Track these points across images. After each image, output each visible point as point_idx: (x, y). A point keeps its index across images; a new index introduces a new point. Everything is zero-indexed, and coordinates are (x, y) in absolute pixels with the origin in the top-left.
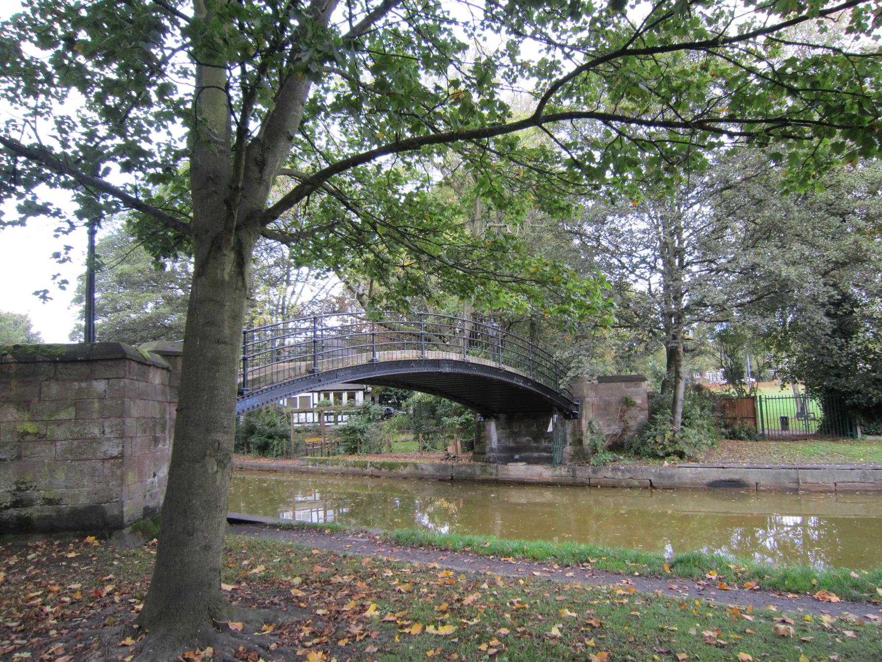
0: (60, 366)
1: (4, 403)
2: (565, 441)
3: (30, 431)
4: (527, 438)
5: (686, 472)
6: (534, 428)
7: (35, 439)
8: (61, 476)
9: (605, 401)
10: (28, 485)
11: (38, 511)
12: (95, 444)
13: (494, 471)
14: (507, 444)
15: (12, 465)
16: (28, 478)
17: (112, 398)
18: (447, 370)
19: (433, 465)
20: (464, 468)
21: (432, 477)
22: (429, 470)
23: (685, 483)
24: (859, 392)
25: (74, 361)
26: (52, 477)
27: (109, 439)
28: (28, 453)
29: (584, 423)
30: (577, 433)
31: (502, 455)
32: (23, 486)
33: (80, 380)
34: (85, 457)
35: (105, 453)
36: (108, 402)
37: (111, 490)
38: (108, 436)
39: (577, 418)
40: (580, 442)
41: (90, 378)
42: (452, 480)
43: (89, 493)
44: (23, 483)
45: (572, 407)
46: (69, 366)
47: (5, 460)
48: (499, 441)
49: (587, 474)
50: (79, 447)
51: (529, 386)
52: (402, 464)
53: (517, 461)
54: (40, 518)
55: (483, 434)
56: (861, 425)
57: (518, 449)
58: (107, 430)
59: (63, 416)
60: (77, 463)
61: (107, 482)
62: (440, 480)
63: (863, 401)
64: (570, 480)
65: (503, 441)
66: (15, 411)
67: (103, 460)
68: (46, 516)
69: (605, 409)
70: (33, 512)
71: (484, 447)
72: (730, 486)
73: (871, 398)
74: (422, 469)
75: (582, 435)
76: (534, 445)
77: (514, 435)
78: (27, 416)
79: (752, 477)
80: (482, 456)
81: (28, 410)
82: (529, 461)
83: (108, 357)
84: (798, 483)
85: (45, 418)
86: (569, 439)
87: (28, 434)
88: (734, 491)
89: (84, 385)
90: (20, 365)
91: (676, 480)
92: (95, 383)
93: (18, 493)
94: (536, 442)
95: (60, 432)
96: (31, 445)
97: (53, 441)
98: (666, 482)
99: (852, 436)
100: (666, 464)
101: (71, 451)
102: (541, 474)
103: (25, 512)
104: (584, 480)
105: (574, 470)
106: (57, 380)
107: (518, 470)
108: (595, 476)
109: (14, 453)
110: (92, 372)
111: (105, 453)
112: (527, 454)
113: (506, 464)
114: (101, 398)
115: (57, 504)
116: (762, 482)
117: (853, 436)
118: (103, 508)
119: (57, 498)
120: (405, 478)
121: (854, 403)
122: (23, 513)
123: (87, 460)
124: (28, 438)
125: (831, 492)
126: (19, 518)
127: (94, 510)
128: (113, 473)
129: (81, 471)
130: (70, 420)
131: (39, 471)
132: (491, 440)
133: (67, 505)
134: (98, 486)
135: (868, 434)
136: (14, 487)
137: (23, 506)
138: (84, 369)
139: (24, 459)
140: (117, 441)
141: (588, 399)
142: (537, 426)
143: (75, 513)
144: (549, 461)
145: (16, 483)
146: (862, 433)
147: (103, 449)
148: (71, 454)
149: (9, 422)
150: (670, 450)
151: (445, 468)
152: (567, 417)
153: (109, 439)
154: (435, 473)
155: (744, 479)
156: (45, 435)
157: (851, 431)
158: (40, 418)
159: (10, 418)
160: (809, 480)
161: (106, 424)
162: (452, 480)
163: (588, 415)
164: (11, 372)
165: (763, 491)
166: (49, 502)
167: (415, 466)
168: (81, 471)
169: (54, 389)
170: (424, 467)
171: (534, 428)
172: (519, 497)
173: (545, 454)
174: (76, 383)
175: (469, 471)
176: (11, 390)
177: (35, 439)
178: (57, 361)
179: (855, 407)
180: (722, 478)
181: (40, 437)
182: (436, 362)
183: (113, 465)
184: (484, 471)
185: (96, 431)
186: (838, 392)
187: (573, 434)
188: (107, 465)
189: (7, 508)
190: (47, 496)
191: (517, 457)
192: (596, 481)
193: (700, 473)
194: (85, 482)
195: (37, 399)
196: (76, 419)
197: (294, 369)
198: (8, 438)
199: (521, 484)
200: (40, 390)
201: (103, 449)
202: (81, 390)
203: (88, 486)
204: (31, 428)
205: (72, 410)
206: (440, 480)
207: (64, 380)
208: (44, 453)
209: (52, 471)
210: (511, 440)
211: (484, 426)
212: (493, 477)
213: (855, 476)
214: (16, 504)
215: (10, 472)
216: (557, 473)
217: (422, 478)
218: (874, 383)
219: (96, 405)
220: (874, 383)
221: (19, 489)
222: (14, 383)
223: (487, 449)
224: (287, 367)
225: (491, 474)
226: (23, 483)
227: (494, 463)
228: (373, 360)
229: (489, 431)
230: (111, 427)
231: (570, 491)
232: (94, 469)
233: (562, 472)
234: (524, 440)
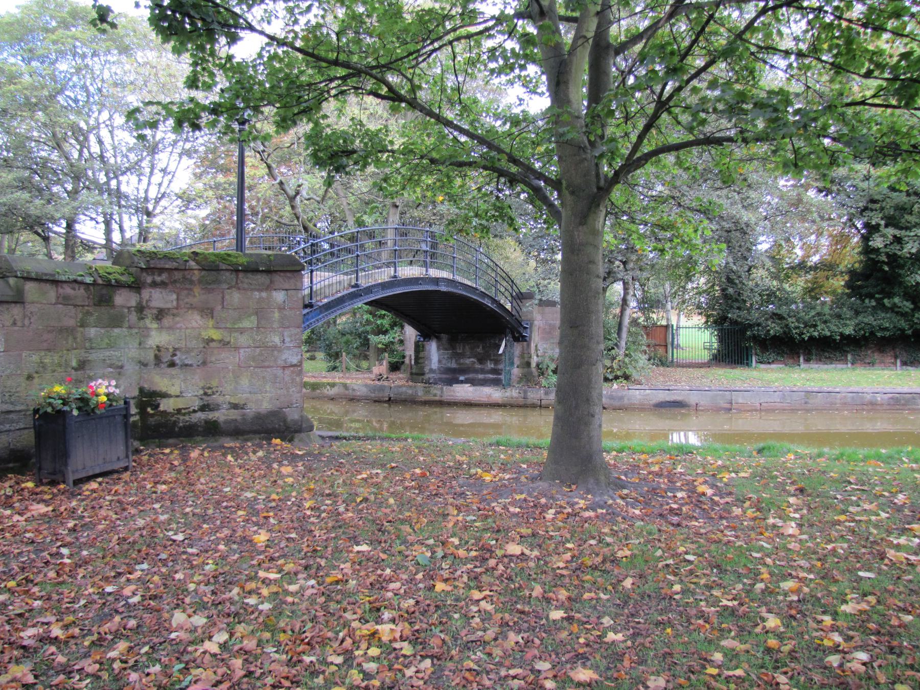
0: (241, 275)
1: (189, 309)
2: (512, 364)
3: (215, 337)
5: (636, 394)
6: (480, 350)
7: (219, 346)
8: (245, 382)
9: (550, 325)
10: (214, 390)
12: (276, 352)
13: (439, 393)
14: (449, 365)
15: (198, 371)
16: (214, 383)
18: (443, 288)
19: (366, 385)
20: (404, 389)
23: (634, 404)
24: (759, 325)
25: (256, 271)
26: (237, 383)
28: (213, 359)
29: (533, 345)
30: (526, 355)
31: (444, 376)
32: (209, 392)
33: (260, 290)
34: (266, 364)
35: (285, 361)
36: (287, 313)
38: (287, 345)
39: (526, 341)
40: (528, 364)
41: (269, 288)
42: (389, 401)
43: (271, 399)
44: (210, 388)
45: (521, 330)
46: (250, 275)
47: (191, 365)
48: (440, 361)
49: (538, 396)
50: (261, 354)
51: (493, 307)
52: (328, 384)
53: (462, 382)
54: (226, 422)
55: (421, 355)
56: (756, 354)
57: (463, 371)
58: (287, 339)
59: (246, 324)
60: (259, 370)
61: (288, 389)
62: (375, 401)
63: (762, 334)
64: (521, 401)
65: (444, 361)
66: (198, 317)
67: (284, 368)
68: (233, 420)
69: (550, 333)
70: (220, 416)
71: (423, 368)
72: (670, 407)
73: (769, 331)
74: (354, 390)
76: (478, 366)
77: (456, 356)
78: (211, 323)
79: (693, 398)
80: (421, 377)
81: (212, 318)
82: (473, 382)
83: (289, 268)
84: (731, 403)
85: (228, 325)
86: (517, 361)
87: (213, 340)
88: (676, 410)
89: (264, 294)
90: (203, 273)
91: (626, 401)
92: (275, 294)
93: (205, 398)
95: (243, 340)
96: (216, 351)
97: (237, 348)
98: (617, 403)
99: (747, 364)
100: (615, 386)
101: (254, 359)
102: (490, 396)
103: (211, 416)
105: (525, 392)
106: (239, 289)
107: (464, 391)
108: (547, 397)
110: (271, 282)
112: (471, 376)
113: (451, 385)
114: (281, 309)
115: (242, 408)
116: (702, 403)
117: (748, 365)
118: (284, 413)
119: (242, 402)
120: (332, 399)
121: (754, 335)
124: (212, 345)
125: (756, 410)
127: (276, 414)
128: (293, 380)
129: (264, 378)
130: (252, 328)
131: (224, 377)
132: (431, 360)
133: (252, 410)
134: (279, 392)
135: (761, 363)
136: (201, 392)
137: (210, 410)
138: (262, 279)
140: (296, 350)
141: (536, 323)
142: (483, 348)
143: (259, 417)
144: (496, 383)
145: (203, 388)
146: (757, 362)
148: (254, 361)
149: (193, 328)
150: (619, 373)
151: (382, 388)
152: (516, 339)
153: (289, 348)
154: (369, 394)
155: (687, 400)
156: (229, 343)
157: (747, 359)
158: (223, 326)
159: (194, 324)
160: (740, 401)
161: (286, 334)
162: (389, 401)
165: (702, 411)
166: (235, 406)
167: (345, 386)
168: (264, 378)
169: (235, 297)
170: (356, 388)
171: (480, 350)
172: (464, 417)
173: (491, 376)
174: (257, 293)
175: (410, 392)
176: (195, 296)
177: (219, 346)
178: (239, 271)
179: (755, 338)
180: (668, 399)
181: (225, 344)
182: (436, 281)
183: (293, 372)
184: (427, 392)
185: (277, 340)
186: (741, 323)
187: (522, 356)
188: (287, 372)
189: (194, 411)
190: (233, 401)
191: (462, 378)
193: (648, 395)
194: (268, 388)
195: (220, 307)
196: (258, 328)
198: (193, 344)
199: (468, 405)
200: (223, 298)
202: (260, 300)
203: (270, 392)
204: (215, 335)
205: (254, 318)
206: (375, 401)
207: (244, 289)
208: (229, 359)
209: (237, 377)
210: (454, 361)
211: (423, 347)
212: (437, 398)
213: (776, 398)
214: (203, 408)
215: (197, 377)
217: (352, 399)
218: (771, 317)
219: (277, 315)
220: (771, 317)
221: (205, 394)
222: (197, 290)
223: (426, 370)
224: (334, 281)
225: (435, 395)
226: (210, 388)
227: (435, 384)
228: (395, 277)
229: (429, 351)
230: (291, 336)
231: (521, 412)
232: (276, 377)
233: (513, 393)
234: (468, 361)
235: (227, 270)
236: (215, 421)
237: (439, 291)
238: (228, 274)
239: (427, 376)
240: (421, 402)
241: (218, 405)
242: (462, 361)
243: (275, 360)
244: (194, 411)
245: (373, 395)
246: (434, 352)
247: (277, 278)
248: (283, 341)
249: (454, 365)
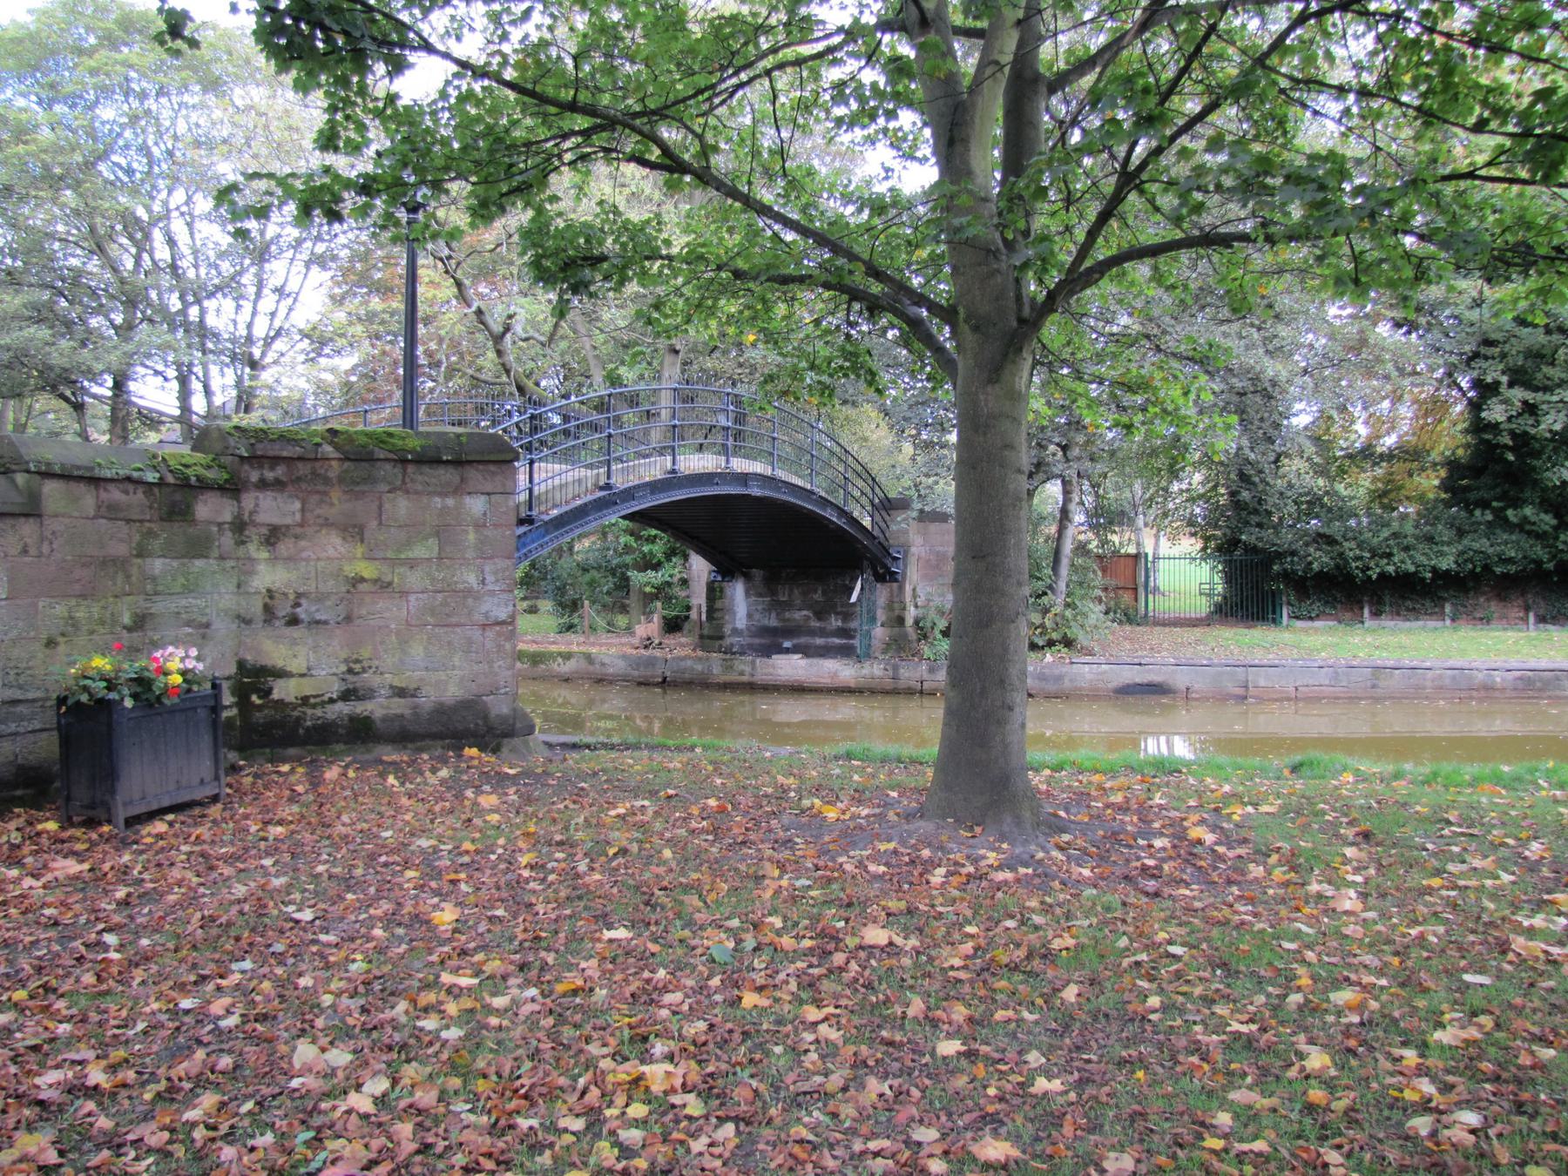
0: (411, 469)
1: (322, 526)
2: (873, 619)
3: (366, 575)
4: (805, 612)
6: (818, 596)
8: (417, 651)
10: (366, 664)
11: (382, 707)
12: (470, 601)
13: (748, 669)
14: (766, 622)
16: (365, 653)
17: (495, 526)
18: (756, 491)
19: (624, 657)
20: (689, 663)
21: (625, 679)
22: (617, 666)
23: (1080, 689)
24: (1293, 553)
25: (437, 462)
27: (492, 593)
28: (364, 612)
29: (908, 588)
31: (757, 641)
32: (357, 667)
33: (443, 495)
34: (454, 620)
35: (486, 615)
37: (496, 674)
38: (490, 587)
39: (896, 581)
40: (901, 621)
41: (459, 490)
43: (462, 679)
44: (357, 661)
45: (888, 562)
46: (426, 469)
47: (326, 623)
48: (749, 616)
49: (918, 675)
50: (445, 604)
51: (841, 522)
52: (560, 654)
53: (788, 651)
54: (385, 719)
55: (718, 604)
56: (1289, 603)
57: (789, 632)
58: (490, 578)
59: (419, 552)
60: (442, 630)
61: (491, 663)
62: (640, 684)
63: (1299, 569)
64: (888, 684)
65: (757, 616)
68: (397, 716)
69: (937, 567)
70: (375, 708)
71: (721, 627)
73: (1310, 563)
74: (603, 664)
75: (904, 609)
76: (815, 624)
77: (778, 606)
78: (360, 550)
79: (1181, 679)
80: (717, 643)
81: (362, 541)
82: (807, 651)
83: (487, 458)
84: (1246, 687)
85: (390, 554)
86: (881, 616)
87: (363, 580)
88: (1153, 699)
89: (450, 502)
90: (347, 464)
91: (1067, 684)
92: (468, 500)
93: (350, 677)
94: (820, 619)
95: (414, 579)
96: (368, 599)
97: (404, 594)
98: (1051, 687)
99: (1274, 621)
100: (1049, 658)
102: (835, 674)
103: (360, 708)
104: (913, 684)
105: (896, 668)
106: (407, 492)
107: (790, 667)
109: (342, 610)
111: (486, 615)
112: (803, 640)
113: (769, 656)
114: (479, 526)
115: (413, 696)
117: (1275, 622)
118: (485, 703)
120: (567, 680)
121: (1285, 570)
122: (358, 710)
123: (457, 625)
124: (363, 587)
125: (1289, 699)
126: (353, 719)
127: (470, 705)
129: (449, 643)
130: (428, 560)
131: (382, 643)
132: (734, 614)
133: (429, 698)
134: (476, 667)
135: (1297, 618)
136: (343, 668)
137: (359, 699)
138: (447, 475)
139: (358, 622)
140: (505, 596)
141: (913, 549)
142: (824, 593)
143: (441, 710)
144: (846, 652)
145: (346, 661)
146: (1290, 617)
147: (484, 608)
148: (433, 615)
150: (1055, 636)
151: (651, 662)
152: (880, 578)
153: (492, 593)
155: (1171, 682)
156: (390, 584)
157: (1274, 612)
158: (380, 555)
159: (331, 552)
160: (1262, 683)
161: (487, 569)
163: (914, 576)
164: (331, 474)
166: (401, 692)
167: (589, 658)
168: (449, 643)
169: (401, 506)
170: (606, 661)
171: (818, 596)
172: (790, 711)
173: (837, 641)
174: (437, 499)
175: (699, 667)
176: (332, 505)
179: (1286, 576)
180: (1138, 680)
181: (383, 586)
182: (744, 478)
183: (499, 634)
184: (729, 668)
185: (472, 579)
186: (1264, 550)
187: (890, 607)
188: (490, 634)
189: (332, 701)
190: (396, 683)
191: (787, 644)
192: (933, 685)
194: (456, 661)
195: (375, 523)
196: (440, 558)
197: (580, 481)
198: (330, 585)
199: (798, 690)
200: (380, 507)
201: (484, 608)
202: (444, 511)
204: (367, 570)
205: (433, 543)
206: (640, 684)
207: (417, 493)
208: (390, 612)
209: (404, 642)
210: (773, 615)
211: (722, 591)
212: (745, 679)
213: (1323, 677)
214: (346, 696)
215: (335, 643)
216: (865, 671)
218: (1315, 541)
219: (472, 537)
220: (1315, 541)
221: (350, 671)
222: (336, 495)
223: (727, 630)
224: (570, 479)
225: (742, 673)
226: (357, 661)
227: (743, 653)
228: (674, 472)
230: (495, 573)
231: (888, 701)
232: (470, 642)
233: (874, 670)
234: (798, 615)
235: (386, 460)
236: (367, 718)
238: (388, 466)
239: (728, 641)
240: (718, 685)
241: (372, 690)
242: (787, 615)
243: (470, 614)
244: (332, 701)
245: (636, 673)
247: (474, 475)
248: (483, 582)
249: (773, 622)
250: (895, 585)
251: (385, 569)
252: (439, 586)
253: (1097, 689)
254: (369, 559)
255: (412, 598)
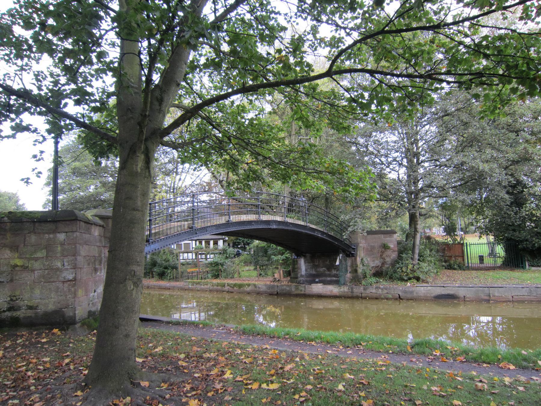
0: (37, 224)
1: (3, 247)
3: (18, 264)
4: (324, 269)
5: (421, 289)
6: (328, 263)
7: (21, 269)
8: (37, 292)
9: (371, 246)
10: (17, 297)
11: (23, 313)
12: (58, 273)
13: (303, 289)
14: (311, 272)
15: (7, 285)
16: (17, 293)
17: (69, 244)
19: (265, 285)
20: (285, 287)
21: (265, 292)
22: (263, 289)
23: (421, 296)
24: (527, 240)
25: (46, 221)
26: (32, 292)
27: (67, 269)
28: (17, 278)
29: (359, 259)
30: (354, 265)
31: (308, 279)
32: (14, 298)
34: (52, 280)
35: (64, 278)
38: (66, 267)
39: (354, 256)
40: (356, 271)
41: (55, 232)
42: (277, 294)
43: (54, 302)
44: (14, 296)
45: (351, 250)
46: (43, 224)
47: (3, 282)
48: (306, 270)
49: (360, 291)
50: (48, 274)
51: (324, 237)
52: (247, 284)
53: (317, 283)
54: (24, 318)
55: (296, 266)
56: (528, 260)
58: (66, 264)
59: (39, 255)
60: (47, 284)
61: (66, 296)
62: (270, 294)
63: (530, 246)
64: (350, 294)
65: (308, 270)
66: (9, 252)
67: (63, 282)
68: (28, 316)
69: (371, 251)
70: (20, 314)
71: (297, 274)
73: (534, 244)
74: (259, 288)
75: (357, 266)
76: (327, 273)
77: (315, 267)
78: (16, 255)
79: (461, 293)
80: (296, 280)
81: (17, 252)
82: (325, 283)
84: (490, 296)
85: (28, 256)
86: (349, 269)
87: (17, 266)
88: (450, 301)
89: (51, 236)
90: (13, 224)
91: (415, 294)
92: (58, 235)
93: (11, 302)
95: (37, 265)
96: (19, 273)
98: (409, 296)
99: (523, 267)
100: (409, 284)
101: (43, 277)
102: (332, 291)
103: (15, 314)
104: (358, 294)
105: (352, 289)
106: (35, 233)
107: (318, 288)
109: (9, 278)
112: (323, 278)
114: (62, 244)
116: (468, 296)
117: (523, 267)
118: (63, 312)
119: (35, 305)
121: (524, 247)
122: (14, 315)
123: (53, 282)
124: (17, 268)
125: (510, 302)
127: (58, 312)
128: (69, 290)
129: (50, 289)
130: (43, 258)
132: (301, 269)
133: (41, 310)
134: (60, 298)
135: (533, 266)
136: (9, 299)
138: (51, 226)
140: (72, 270)
141: (360, 245)
142: (330, 261)
143: (46, 314)
144: (337, 283)
145: (10, 296)
146: (529, 266)
148: (43, 278)
150: (411, 276)
151: (273, 287)
153: (67, 269)
155: (457, 294)
156: (27, 267)
157: (522, 264)
158: (24, 257)
159: (6, 256)
160: (496, 294)
161: (65, 260)
162: (277, 294)
163: (361, 254)
164: (7, 228)
165: (468, 301)
166: (30, 308)
167: (255, 286)
169: (33, 239)
170: (260, 286)
171: (328, 263)
172: (318, 305)
173: (334, 279)
174: (47, 235)
175: (288, 289)
176: (7, 239)
177: (21, 269)
179: (524, 249)
180: (443, 293)
181: (25, 268)
182: (268, 222)
183: (69, 285)
184: (297, 289)
185: (59, 264)
187: (352, 266)
188: (66, 285)
189: (4, 311)
190: (29, 304)
191: (317, 280)
192: (366, 295)
193: (429, 290)
194: (52, 295)
195: (23, 245)
196: (47, 257)
197: (181, 226)
198: (5, 268)
199: (320, 296)
200: (25, 239)
202: (49, 239)
203: (54, 298)
204: (19, 262)
205: (44, 251)
206: (270, 294)
207: (39, 233)
208: (27, 278)
209: (32, 289)
210: (314, 270)
211: (297, 261)
212: (303, 292)
213: (524, 292)
214: (10, 309)
215: (6, 289)
216: (342, 290)
217: (259, 293)
218: (536, 235)
219: (59, 248)
220: (536, 235)
221: (12, 300)
222: (8, 235)
223: (299, 276)
225: (301, 291)
226: (14, 296)
227: (303, 284)
228: (229, 221)
229: (300, 264)
230: (68, 262)
231: (350, 301)
232: (58, 288)
233: (345, 289)
234: (322, 270)
235: (26, 222)
236: (17, 318)
237: (270, 228)
238: (28, 224)
239: (299, 279)
240: (294, 295)
241: (20, 307)
242: (318, 269)
243: (58, 278)
244: (4, 311)
245: (269, 291)
246: (303, 265)
247: (61, 226)
248: (64, 265)
249: (314, 272)
250: (353, 258)
251: (26, 261)
252: (46, 267)
253: (427, 297)
254: (20, 258)
255: (36, 272)
